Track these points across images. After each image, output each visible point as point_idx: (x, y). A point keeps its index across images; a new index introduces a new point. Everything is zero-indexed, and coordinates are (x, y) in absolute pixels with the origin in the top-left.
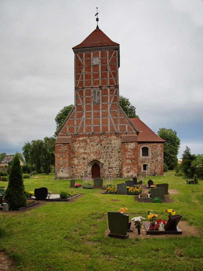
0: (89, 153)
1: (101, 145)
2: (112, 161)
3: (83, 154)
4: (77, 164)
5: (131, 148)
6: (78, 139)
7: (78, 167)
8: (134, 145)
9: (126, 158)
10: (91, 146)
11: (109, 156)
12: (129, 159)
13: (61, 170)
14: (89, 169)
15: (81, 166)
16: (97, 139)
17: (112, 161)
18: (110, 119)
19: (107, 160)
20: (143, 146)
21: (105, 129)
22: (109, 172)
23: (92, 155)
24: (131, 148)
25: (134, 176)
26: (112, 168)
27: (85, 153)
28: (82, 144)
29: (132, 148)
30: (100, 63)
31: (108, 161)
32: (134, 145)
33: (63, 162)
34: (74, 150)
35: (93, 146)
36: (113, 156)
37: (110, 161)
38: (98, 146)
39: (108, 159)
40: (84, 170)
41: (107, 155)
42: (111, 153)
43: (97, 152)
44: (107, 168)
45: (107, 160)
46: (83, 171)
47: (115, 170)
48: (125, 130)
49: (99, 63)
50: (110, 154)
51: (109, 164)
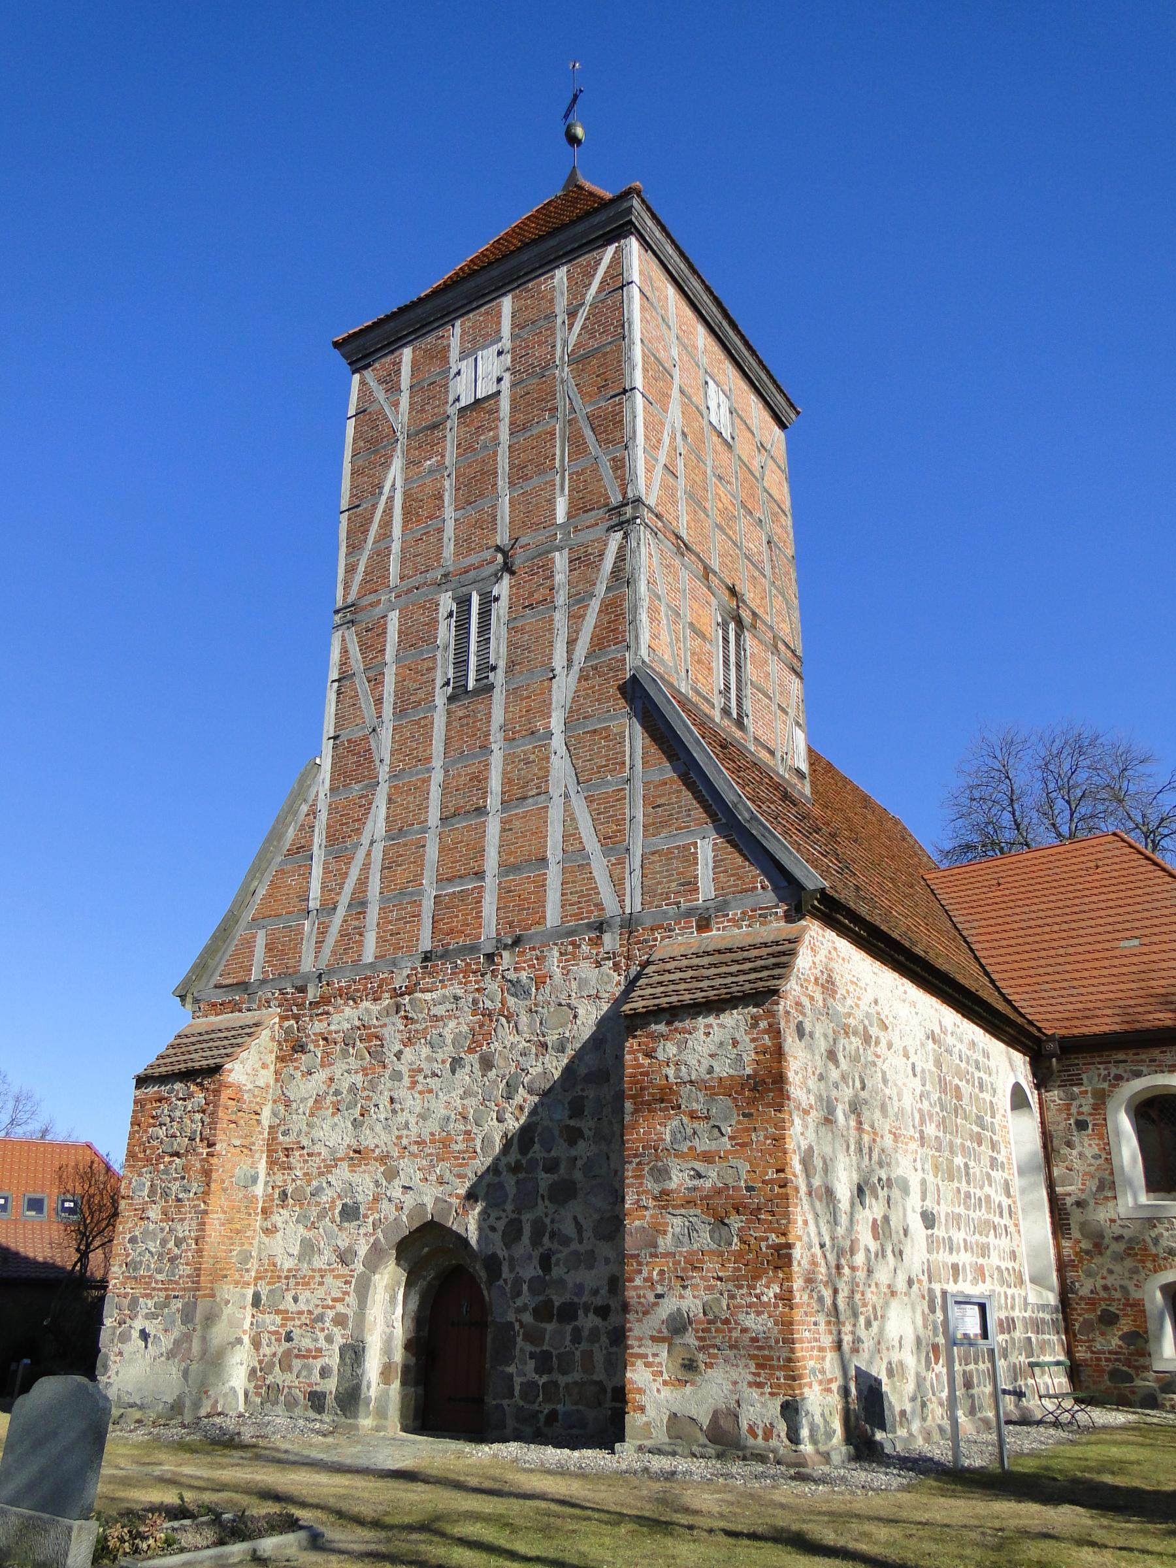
0: (384, 1159)
1: (487, 1063)
2: (569, 1229)
3: (343, 1172)
4: (289, 1264)
5: (711, 1070)
6: (318, 1027)
7: (296, 1300)
8: (741, 1035)
9: (665, 1193)
10: (406, 1081)
11: (545, 1180)
12: (689, 1203)
13: (139, 1324)
14: (386, 1318)
15: (321, 1292)
16: (446, 1000)
17: (569, 1229)
18: (566, 812)
19: (526, 1217)
20: (1137, 1085)
21: (521, 906)
22: (544, 1363)
23: (410, 1171)
24: (711, 1070)
25: (752, 1431)
26: (568, 1313)
27: (359, 1155)
28: (346, 1072)
29: (723, 1069)
30: (507, 377)
31: (539, 1231)
32: (741, 1035)
33: (164, 1242)
34: (284, 1134)
35: (420, 1078)
36: (578, 1175)
37: (553, 1235)
38: (463, 1075)
39: (540, 1210)
40: (337, 1332)
41: (533, 1163)
42: (560, 1150)
43: (445, 1143)
44: (528, 1318)
45: (526, 1217)
46: (329, 1339)
47: (594, 1335)
48: (691, 886)
49: (499, 380)
50: (553, 1154)
51: (546, 1262)
